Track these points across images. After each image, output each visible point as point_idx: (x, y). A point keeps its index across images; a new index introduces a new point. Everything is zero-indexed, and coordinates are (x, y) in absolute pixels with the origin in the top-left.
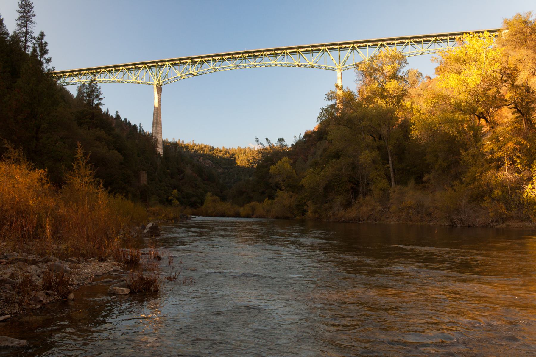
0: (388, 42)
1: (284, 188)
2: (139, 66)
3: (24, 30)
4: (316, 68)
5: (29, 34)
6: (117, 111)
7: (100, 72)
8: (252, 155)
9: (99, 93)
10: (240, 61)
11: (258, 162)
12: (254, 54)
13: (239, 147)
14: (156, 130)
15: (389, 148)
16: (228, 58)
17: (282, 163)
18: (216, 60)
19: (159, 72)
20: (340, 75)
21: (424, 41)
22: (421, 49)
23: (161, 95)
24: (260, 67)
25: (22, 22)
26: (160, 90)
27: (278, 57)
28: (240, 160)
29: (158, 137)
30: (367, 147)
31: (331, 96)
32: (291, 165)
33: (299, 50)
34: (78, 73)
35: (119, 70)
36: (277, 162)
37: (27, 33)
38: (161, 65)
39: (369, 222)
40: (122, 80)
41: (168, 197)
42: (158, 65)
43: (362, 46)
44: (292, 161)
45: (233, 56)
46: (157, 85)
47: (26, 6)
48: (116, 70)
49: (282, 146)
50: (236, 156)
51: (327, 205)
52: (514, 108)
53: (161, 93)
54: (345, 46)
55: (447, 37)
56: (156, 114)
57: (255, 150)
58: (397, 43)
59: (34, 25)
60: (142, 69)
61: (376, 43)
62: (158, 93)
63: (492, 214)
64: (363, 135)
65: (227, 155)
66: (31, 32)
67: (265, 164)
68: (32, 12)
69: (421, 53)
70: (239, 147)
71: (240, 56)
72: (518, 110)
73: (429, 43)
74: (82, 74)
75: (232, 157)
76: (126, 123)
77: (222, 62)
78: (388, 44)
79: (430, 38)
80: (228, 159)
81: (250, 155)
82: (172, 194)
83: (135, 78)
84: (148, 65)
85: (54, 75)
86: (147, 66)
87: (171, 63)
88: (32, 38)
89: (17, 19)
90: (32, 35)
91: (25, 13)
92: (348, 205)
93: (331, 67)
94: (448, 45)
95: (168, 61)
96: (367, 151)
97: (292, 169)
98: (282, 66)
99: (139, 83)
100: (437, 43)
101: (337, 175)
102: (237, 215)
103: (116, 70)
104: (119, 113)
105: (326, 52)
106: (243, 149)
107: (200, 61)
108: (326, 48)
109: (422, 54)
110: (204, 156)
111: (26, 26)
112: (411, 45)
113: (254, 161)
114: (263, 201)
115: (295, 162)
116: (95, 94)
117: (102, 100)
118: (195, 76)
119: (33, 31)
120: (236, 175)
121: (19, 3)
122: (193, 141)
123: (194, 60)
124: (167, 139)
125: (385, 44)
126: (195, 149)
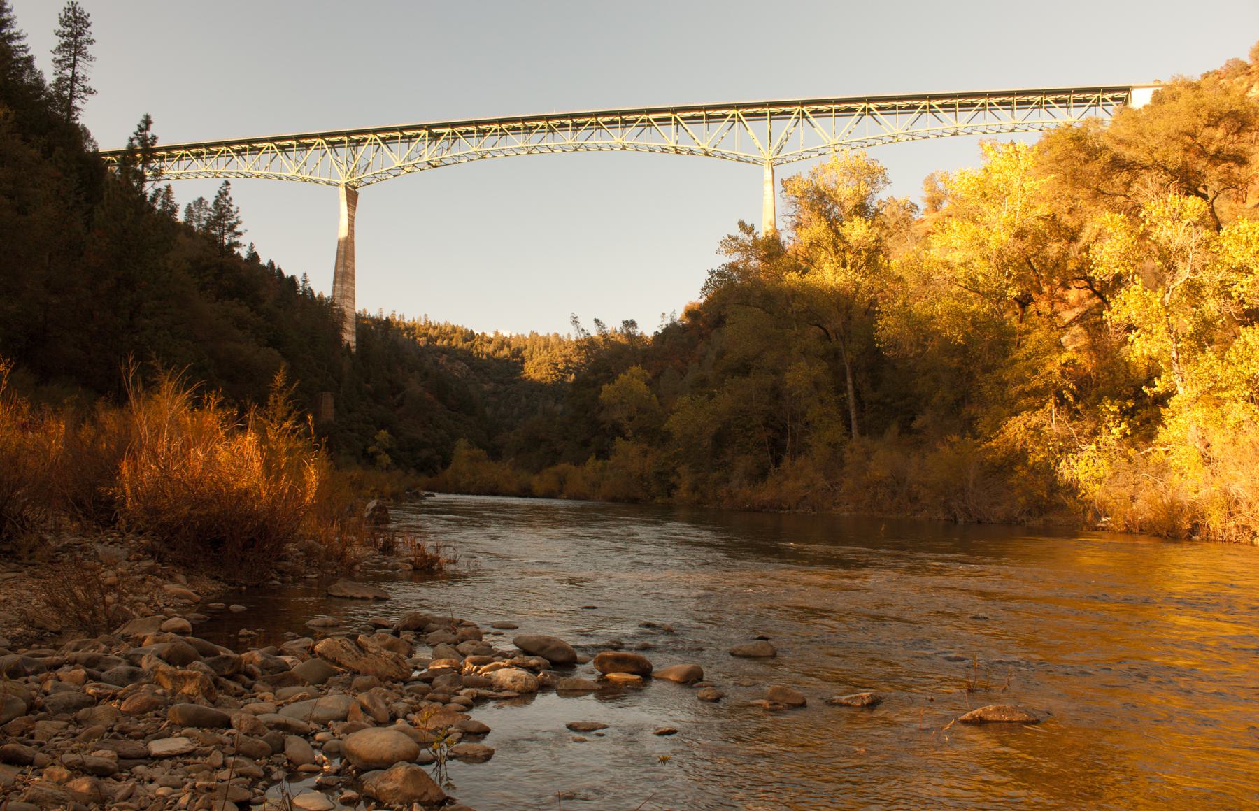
0: (880, 104)
1: (630, 434)
2: (308, 141)
3: (69, 72)
4: (715, 156)
5: (80, 81)
7: (217, 152)
8: (563, 353)
9: (235, 221)
10: (541, 135)
11: (577, 371)
12: (574, 120)
13: (532, 332)
15: (848, 358)
16: (514, 129)
18: (485, 132)
19: (354, 156)
20: (771, 176)
21: (960, 106)
22: (955, 122)
23: (355, 210)
25: (64, 57)
26: (353, 203)
27: (628, 130)
28: (535, 363)
29: (347, 307)
30: (804, 353)
31: (731, 243)
32: (649, 383)
33: (677, 115)
34: (165, 153)
35: (260, 149)
37: (74, 79)
38: (358, 141)
40: (266, 173)
41: (368, 446)
42: (351, 141)
43: (821, 112)
44: (649, 376)
45: (525, 124)
46: (346, 187)
47: (75, 22)
49: (631, 337)
50: (526, 353)
51: (716, 475)
52: (1086, 287)
53: (355, 204)
54: (783, 108)
55: (1012, 98)
56: (342, 254)
58: (900, 108)
59: (89, 63)
61: (852, 106)
62: (348, 206)
63: (1022, 500)
64: (796, 329)
65: (505, 352)
66: (84, 78)
68: (88, 34)
70: (532, 332)
71: (541, 123)
73: (971, 110)
74: (175, 156)
75: (517, 357)
76: (272, 273)
77: (498, 137)
78: (879, 109)
79: (973, 100)
80: (505, 361)
82: (375, 441)
83: (297, 169)
84: (327, 139)
85: (109, 158)
86: (326, 141)
87: (382, 135)
88: (84, 91)
89: (53, 49)
90: (84, 83)
91: (72, 36)
92: (761, 475)
93: (751, 155)
94: (1015, 115)
96: (801, 364)
99: (305, 181)
100: (990, 110)
101: (741, 411)
102: (526, 492)
103: (253, 149)
104: (257, 249)
105: (739, 121)
106: (544, 338)
107: (449, 134)
108: (740, 112)
109: (955, 134)
110: (450, 352)
111: (73, 66)
112: (932, 112)
113: (567, 367)
114: (584, 460)
115: (656, 377)
116: (226, 222)
118: (435, 167)
119: (88, 75)
120: (524, 400)
121: (60, 14)
122: (426, 315)
123: (434, 131)
124: (365, 311)
125: (872, 108)
126: (431, 336)
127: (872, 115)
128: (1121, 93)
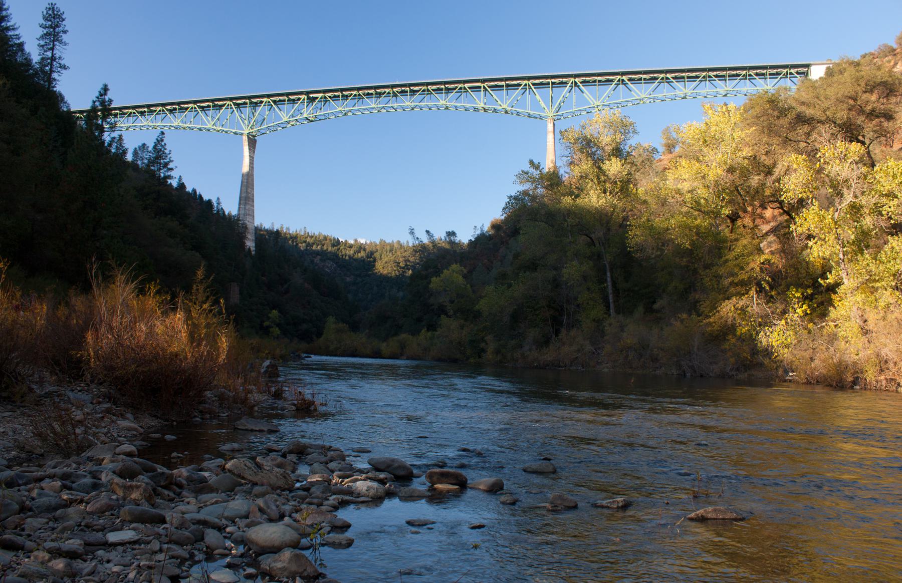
0: (630, 76)
1: (451, 313)
3: (49, 54)
4: (512, 114)
5: (57, 60)
6: (180, 176)
8: (404, 254)
9: (168, 160)
10: (388, 99)
11: (413, 268)
12: (412, 88)
13: (381, 240)
14: (245, 209)
15: (608, 258)
16: (368, 94)
17: (450, 273)
18: (347, 96)
19: (253, 114)
20: (552, 128)
21: (688, 78)
22: (684, 90)
23: (254, 152)
24: (421, 109)
25: (46, 42)
28: (384, 262)
32: (465, 277)
33: (486, 84)
34: (118, 112)
35: (187, 109)
36: (442, 273)
37: (53, 58)
38: (256, 103)
39: (573, 368)
40: (190, 126)
41: (264, 322)
42: (251, 103)
43: (588, 82)
44: (465, 271)
46: (248, 136)
47: (54, 18)
48: (181, 109)
49: (452, 243)
50: (377, 255)
53: (254, 148)
55: (725, 72)
57: (408, 246)
58: (645, 79)
59: (64, 47)
60: (224, 108)
62: (250, 149)
63: (732, 360)
65: (362, 254)
66: (60, 58)
67: (424, 273)
69: (683, 96)
70: (381, 240)
71: (387, 90)
72: (785, 211)
73: (696, 81)
75: (371, 257)
76: (195, 197)
77: (357, 100)
78: (630, 80)
79: (697, 73)
80: (362, 261)
81: (400, 255)
82: (269, 318)
83: (213, 123)
84: (234, 101)
88: (60, 67)
89: (38, 37)
90: (60, 62)
92: (545, 342)
94: (727, 84)
95: (269, 96)
97: (465, 283)
98: (456, 109)
99: (218, 131)
100: (709, 81)
102: (377, 355)
103: (181, 109)
104: (184, 180)
105: (529, 88)
106: (390, 244)
107: (321, 98)
108: (530, 82)
109: (684, 98)
110: (323, 254)
111: (52, 49)
112: (668, 82)
113: (406, 265)
115: (470, 272)
116: (162, 161)
117: (173, 171)
118: (312, 121)
119: (63, 56)
121: (43, 12)
123: (311, 96)
126: (309, 243)
127: (625, 84)
128: (803, 69)
